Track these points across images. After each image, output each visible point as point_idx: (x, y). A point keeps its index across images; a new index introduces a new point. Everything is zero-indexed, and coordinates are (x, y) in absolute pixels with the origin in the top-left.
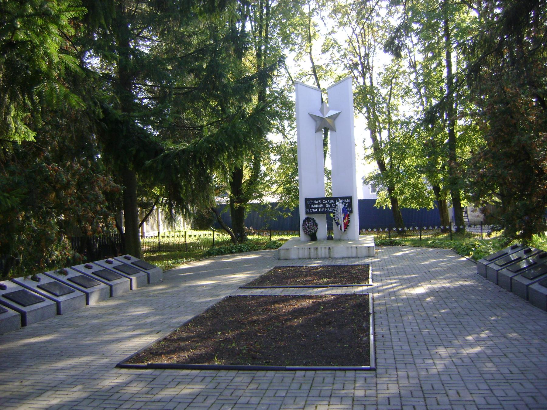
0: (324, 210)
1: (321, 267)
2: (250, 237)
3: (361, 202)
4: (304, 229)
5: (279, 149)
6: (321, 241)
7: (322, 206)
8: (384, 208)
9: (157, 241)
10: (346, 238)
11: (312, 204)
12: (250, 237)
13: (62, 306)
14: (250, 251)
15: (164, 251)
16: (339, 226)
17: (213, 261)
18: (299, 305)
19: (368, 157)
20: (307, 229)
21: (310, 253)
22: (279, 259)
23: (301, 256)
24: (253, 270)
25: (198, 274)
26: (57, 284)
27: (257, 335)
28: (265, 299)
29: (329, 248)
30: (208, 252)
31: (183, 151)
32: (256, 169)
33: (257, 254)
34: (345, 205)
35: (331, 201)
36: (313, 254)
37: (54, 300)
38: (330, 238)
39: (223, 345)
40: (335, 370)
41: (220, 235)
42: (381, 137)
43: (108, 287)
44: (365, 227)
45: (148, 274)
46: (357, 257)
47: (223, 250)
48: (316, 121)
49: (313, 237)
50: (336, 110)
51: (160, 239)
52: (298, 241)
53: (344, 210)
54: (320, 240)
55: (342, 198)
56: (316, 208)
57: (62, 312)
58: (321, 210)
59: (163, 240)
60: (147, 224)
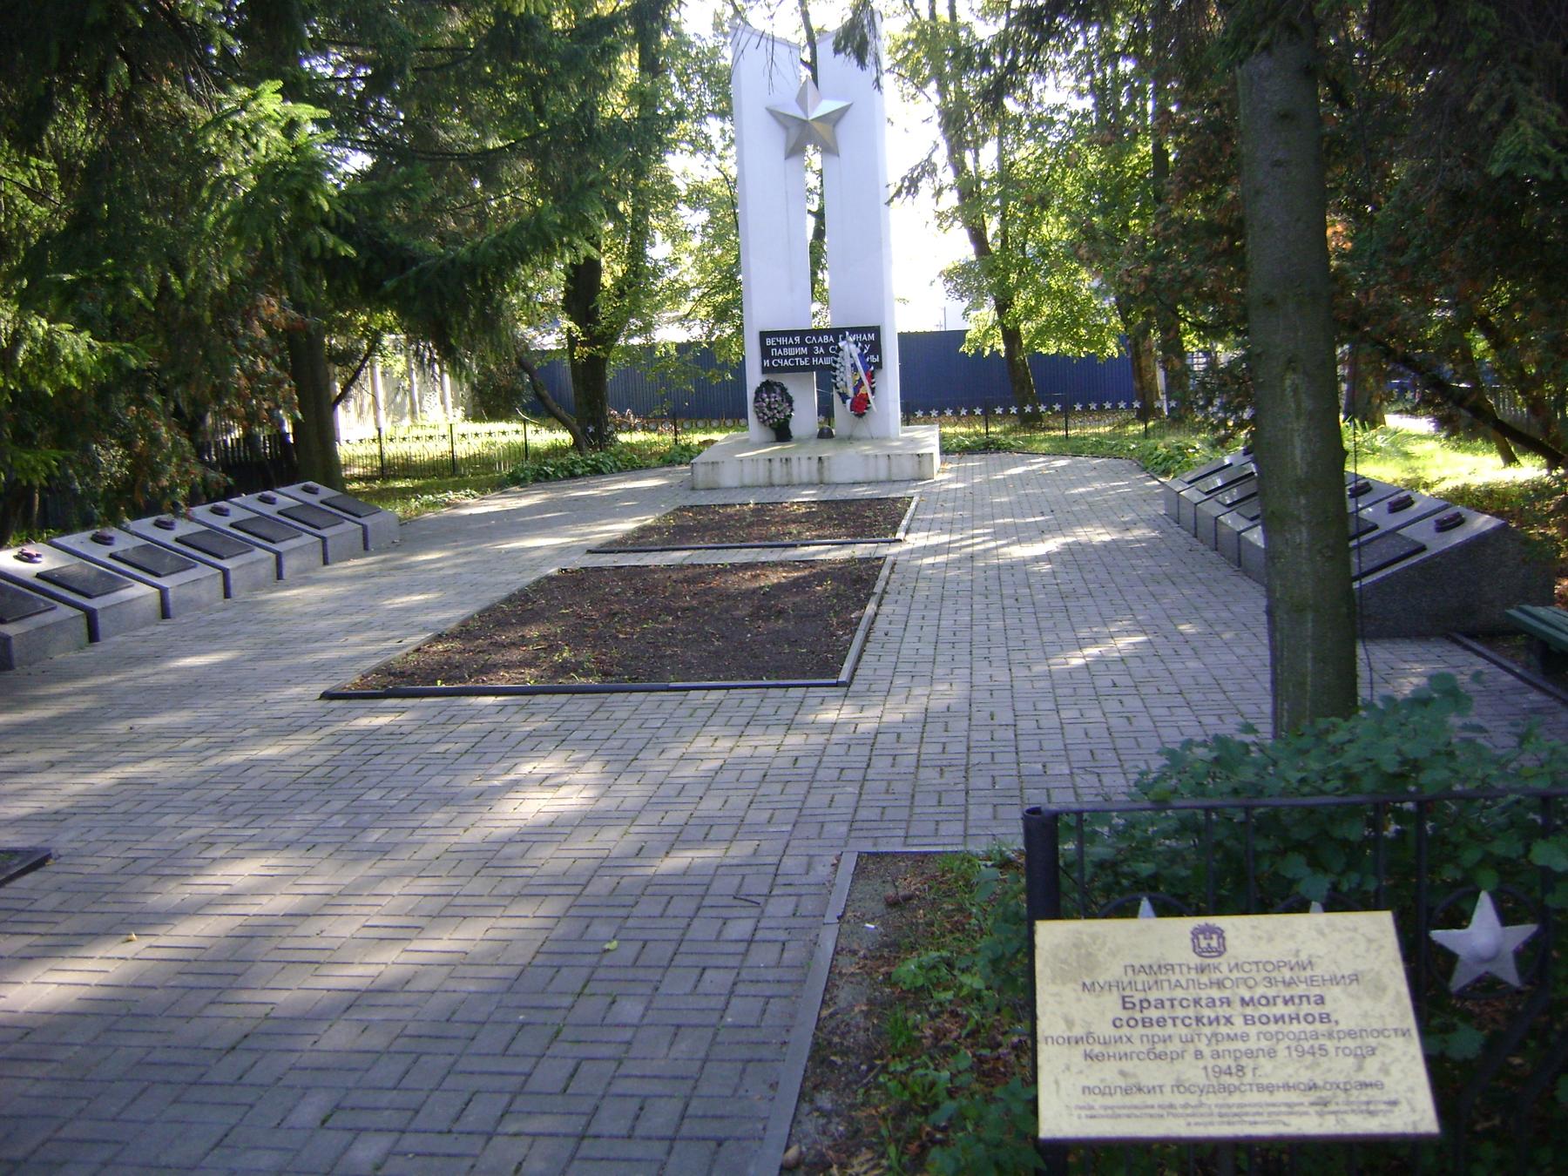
0: (810, 361)
2: (623, 438)
3: (904, 338)
5: (697, 197)
6: (802, 441)
7: (805, 351)
8: (987, 353)
10: (865, 433)
11: (779, 346)
12: (623, 438)
14: (620, 470)
20: (766, 411)
21: (770, 471)
22: (693, 489)
23: (747, 481)
26: (153, 547)
27: (617, 637)
29: (820, 459)
30: (511, 475)
32: (636, 255)
34: (862, 350)
35: (826, 339)
36: (778, 477)
38: (825, 434)
40: (768, 687)
42: (976, 160)
45: (365, 528)
47: (550, 470)
48: (786, 128)
49: (782, 432)
50: (836, 98)
54: (799, 440)
55: (853, 331)
56: (788, 357)
57: (172, 612)
58: (802, 363)
59: (391, 450)
60: (345, 408)
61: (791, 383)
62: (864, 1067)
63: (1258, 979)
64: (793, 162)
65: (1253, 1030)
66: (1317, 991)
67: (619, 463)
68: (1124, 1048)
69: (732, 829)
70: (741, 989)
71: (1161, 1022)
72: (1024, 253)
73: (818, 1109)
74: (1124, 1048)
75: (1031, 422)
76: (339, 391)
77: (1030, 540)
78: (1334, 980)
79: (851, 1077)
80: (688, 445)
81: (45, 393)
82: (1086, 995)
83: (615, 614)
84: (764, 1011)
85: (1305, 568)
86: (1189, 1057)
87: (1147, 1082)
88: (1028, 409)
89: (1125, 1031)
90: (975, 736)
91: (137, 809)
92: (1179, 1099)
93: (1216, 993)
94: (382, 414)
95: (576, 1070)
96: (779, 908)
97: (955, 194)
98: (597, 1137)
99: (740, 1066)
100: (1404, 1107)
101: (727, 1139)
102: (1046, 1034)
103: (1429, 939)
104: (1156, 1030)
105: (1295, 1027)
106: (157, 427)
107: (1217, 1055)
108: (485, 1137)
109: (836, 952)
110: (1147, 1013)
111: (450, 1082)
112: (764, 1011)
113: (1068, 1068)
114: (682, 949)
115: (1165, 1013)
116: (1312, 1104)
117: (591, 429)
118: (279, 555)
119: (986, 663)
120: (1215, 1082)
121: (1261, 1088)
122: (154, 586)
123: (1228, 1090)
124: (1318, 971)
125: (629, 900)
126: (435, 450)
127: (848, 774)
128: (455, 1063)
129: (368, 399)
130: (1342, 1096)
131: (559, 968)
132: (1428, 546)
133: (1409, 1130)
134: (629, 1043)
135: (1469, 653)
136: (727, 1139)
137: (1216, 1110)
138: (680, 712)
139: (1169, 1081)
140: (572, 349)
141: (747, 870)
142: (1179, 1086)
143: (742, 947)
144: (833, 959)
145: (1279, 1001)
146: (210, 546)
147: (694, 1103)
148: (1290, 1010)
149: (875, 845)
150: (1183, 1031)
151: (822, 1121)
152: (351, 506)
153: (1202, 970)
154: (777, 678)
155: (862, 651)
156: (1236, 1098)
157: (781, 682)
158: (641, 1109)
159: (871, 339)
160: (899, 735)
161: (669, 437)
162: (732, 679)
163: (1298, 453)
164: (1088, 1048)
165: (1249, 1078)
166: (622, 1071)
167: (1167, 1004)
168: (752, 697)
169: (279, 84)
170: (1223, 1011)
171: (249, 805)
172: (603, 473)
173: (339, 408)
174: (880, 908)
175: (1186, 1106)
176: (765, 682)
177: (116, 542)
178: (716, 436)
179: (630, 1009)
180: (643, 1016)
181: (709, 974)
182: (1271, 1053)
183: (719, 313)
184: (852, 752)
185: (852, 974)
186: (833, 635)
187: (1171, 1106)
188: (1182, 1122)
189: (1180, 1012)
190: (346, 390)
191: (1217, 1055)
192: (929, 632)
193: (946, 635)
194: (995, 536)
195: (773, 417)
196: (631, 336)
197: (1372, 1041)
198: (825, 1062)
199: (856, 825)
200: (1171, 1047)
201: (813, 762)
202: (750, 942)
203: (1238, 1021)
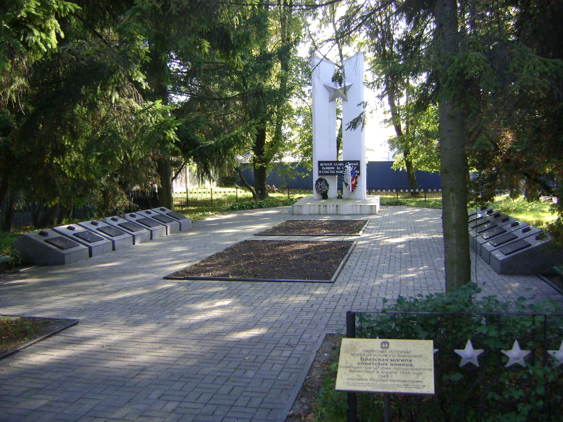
0: (335, 172)
1: (326, 221)
2: (271, 195)
3: (371, 165)
4: (317, 188)
7: (333, 168)
8: (401, 169)
9: (186, 197)
11: (324, 166)
12: (271, 195)
13: (116, 244)
14: (268, 207)
15: (192, 206)
16: (348, 186)
17: (235, 215)
18: (296, 247)
19: (385, 121)
22: (293, 214)
23: (312, 212)
24: (269, 223)
25: (221, 224)
28: (273, 243)
29: (337, 206)
30: (231, 207)
31: (210, 145)
32: (278, 132)
33: (276, 210)
34: (353, 168)
37: (110, 240)
38: (340, 197)
39: (236, 268)
41: (243, 191)
43: (150, 232)
44: (372, 188)
45: (180, 223)
46: (361, 215)
47: (244, 206)
48: (330, 91)
49: (325, 196)
51: (188, 194)
52: (311, 199)
53: (352, 172)
54: (331, 199)
55: (351, 162)
56: (328, 170)
57: (116, 249)
58: (332, 172)
59: (190, 196)
60: (176, 181)
61: (328, 179)
62: (316, 392)
63: (396, 355)
64: (332, 103)
65: (392, 367)
66: (410, 359)
67: (268, 204)
68: (360, 369)
69: (289, 325)
70: (284, 370)
71: (370, 364)
72: (414, 135)
73: (301, 402)
74: (360, 369)
75: (415, 195)
76: (174, 176)
77: (397, 237)
78: (415, 356)
79: (312, 394)
80: (293, 199)
81: (84, 179)
82: (352, 357)
83: (261, 256)
84: (290, 377)
85: (455, 251)
86: (375, 373)
87: (364, 377)
88: (412, 191)
89: (361, 365)
90: (371, 300)
91: (105, 310)
92: (371, 382)
93: (384, 358)
94: (188, 184)
95: (232, 389)
96: (300, 348)
97: (390, 113)
98: (236, 406)
99: (280, 390)
100: (427, 387)
101: (274, 409)
102: (341, 365)
103: (454, 352)
104: (368, 366)
105: (403, 367)
106: (116, 188)
107: (382, 372)
108: (204, 405)
109: (314, 361)
110: (366, 362)
111: (196, 390)
112: (290, 377)
113: (345, 373)
114: (268, 358)
115: (371, 362)
116: (404, 385)
117: (260, 192)
118: (151, 231)
119: (380, 277)
120: (380, 379)
121: (392, 381)
122: (110, 240)
123: (383, 381)
124: (412, 354)
125: (255, 344)
126: (207, 196)
127: (328, 310)
128: (198, 385)
129: (184, 178)
130: (411, 384)
131: (231, 361)
132: (531, 244)
133: (427, 392)
134: (249, 383)
135: (542, 281)
136: (274, 409)
137: (380, 385)
138: (278, 289)
139: (369, 378)
140: (254, 164)
141: (292, 337)
142: (371, 379)
143: (286, 359)
144: (313, 363)
145: (400, 361)
146: (125, 227)
147: (266, 399)
148: (403, 363)
149: (333, 331)
150: (375, 366)
151: (301, 405)
152: (177, 216)
153: (382, 352)
154: (311, 279)
155: (340, 272)
156: (385, 383)
157: (312, 281)
158: (250, 400)
159: (356, 165)
160: (347, 299)
161: (287, 195)
162: (296, 279)
163: (453, 216)
164: (350, 369)
165: (389, 378)
166: (246, 389)
167: (372, 360)
168: (301, 285)
169: (161, 101)
170: (385, 362)
171: (140, 310)
172: (263, 208)
173: (174, 181)
174: (329, 349)
175: (372, 384)
176: (307, 280)
177: (99, 225)
178: (303, 195)
179: (250, 374)
180: (254, 376)
181: (275, 365)
182: (396, 373)
183: (305, 153)
184: (331, 304)
185: (318, 367)
186: (331, 266)
187: (369, 384)
188: (371, 388)
189: (375, 362)
190: (176, 175)
191: (382, 372)
192: (364, 266)
193: (369, 268)
194: (386, 235)
195: (322, 191)
196: (275, 160)
197: (422, 371)
198: (305, 390)
199: (328, 326)
200: (371, 370)
201: (318, 306)
202: (289, 357)
203: (389, 365)
